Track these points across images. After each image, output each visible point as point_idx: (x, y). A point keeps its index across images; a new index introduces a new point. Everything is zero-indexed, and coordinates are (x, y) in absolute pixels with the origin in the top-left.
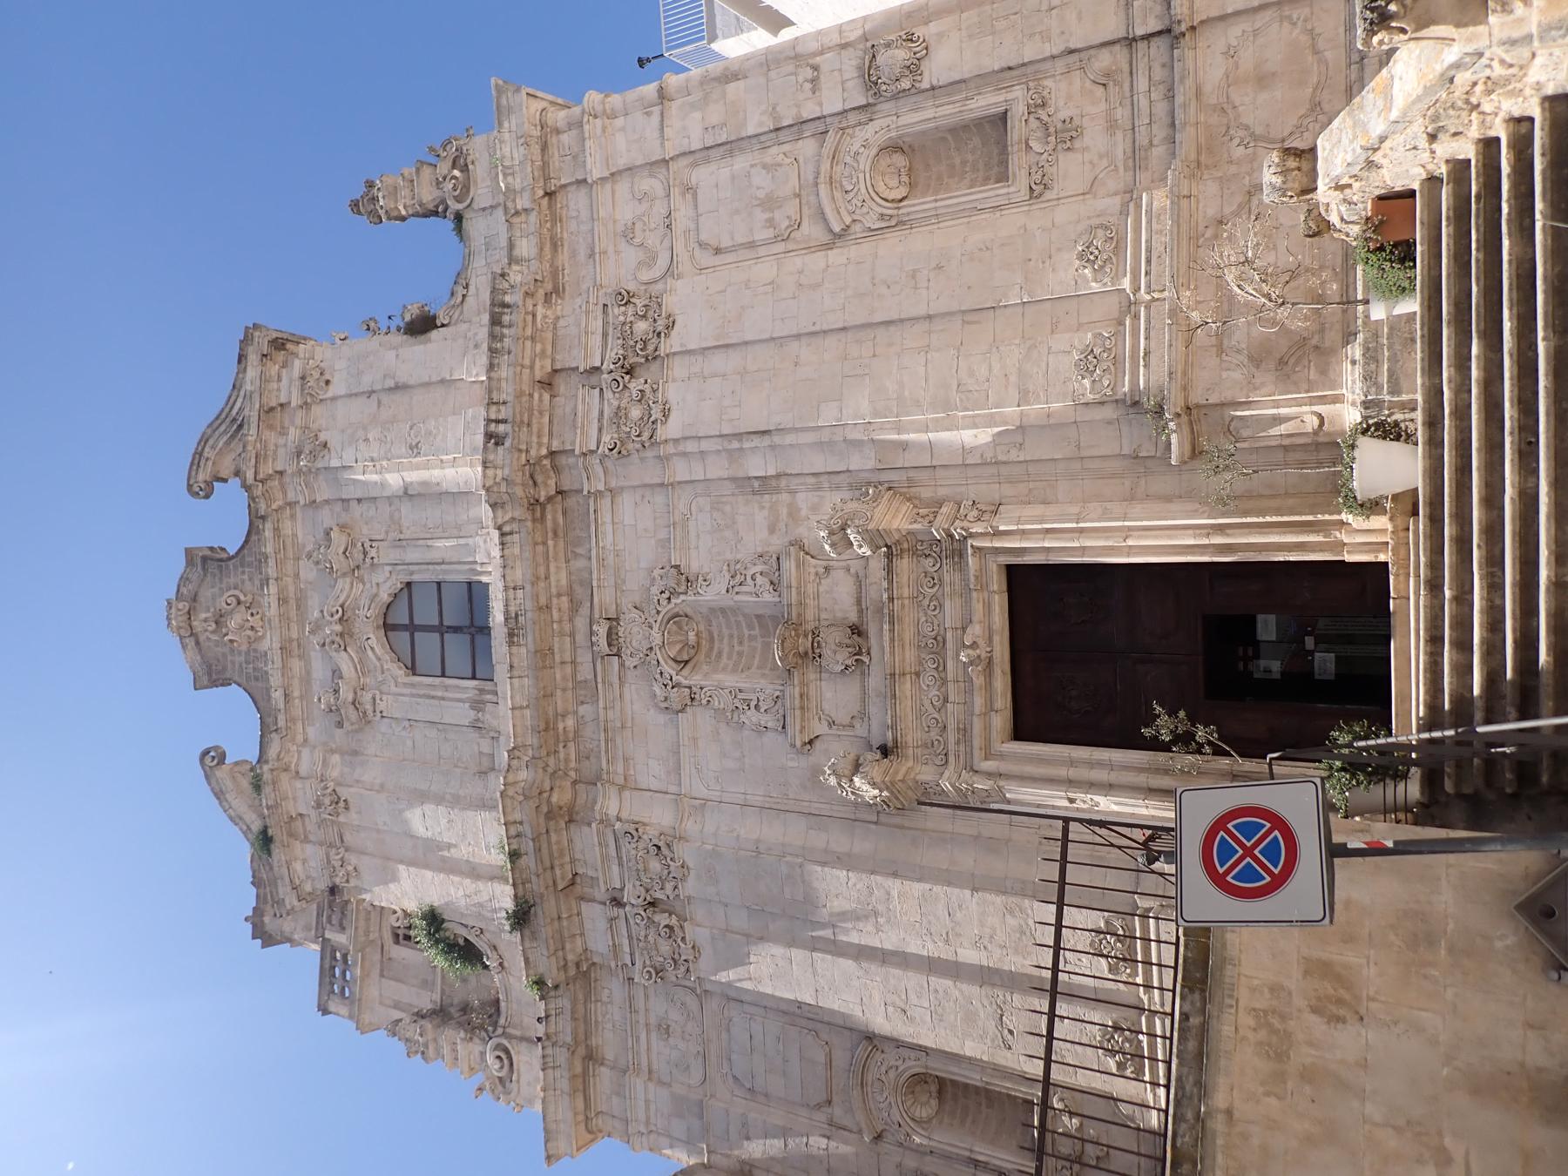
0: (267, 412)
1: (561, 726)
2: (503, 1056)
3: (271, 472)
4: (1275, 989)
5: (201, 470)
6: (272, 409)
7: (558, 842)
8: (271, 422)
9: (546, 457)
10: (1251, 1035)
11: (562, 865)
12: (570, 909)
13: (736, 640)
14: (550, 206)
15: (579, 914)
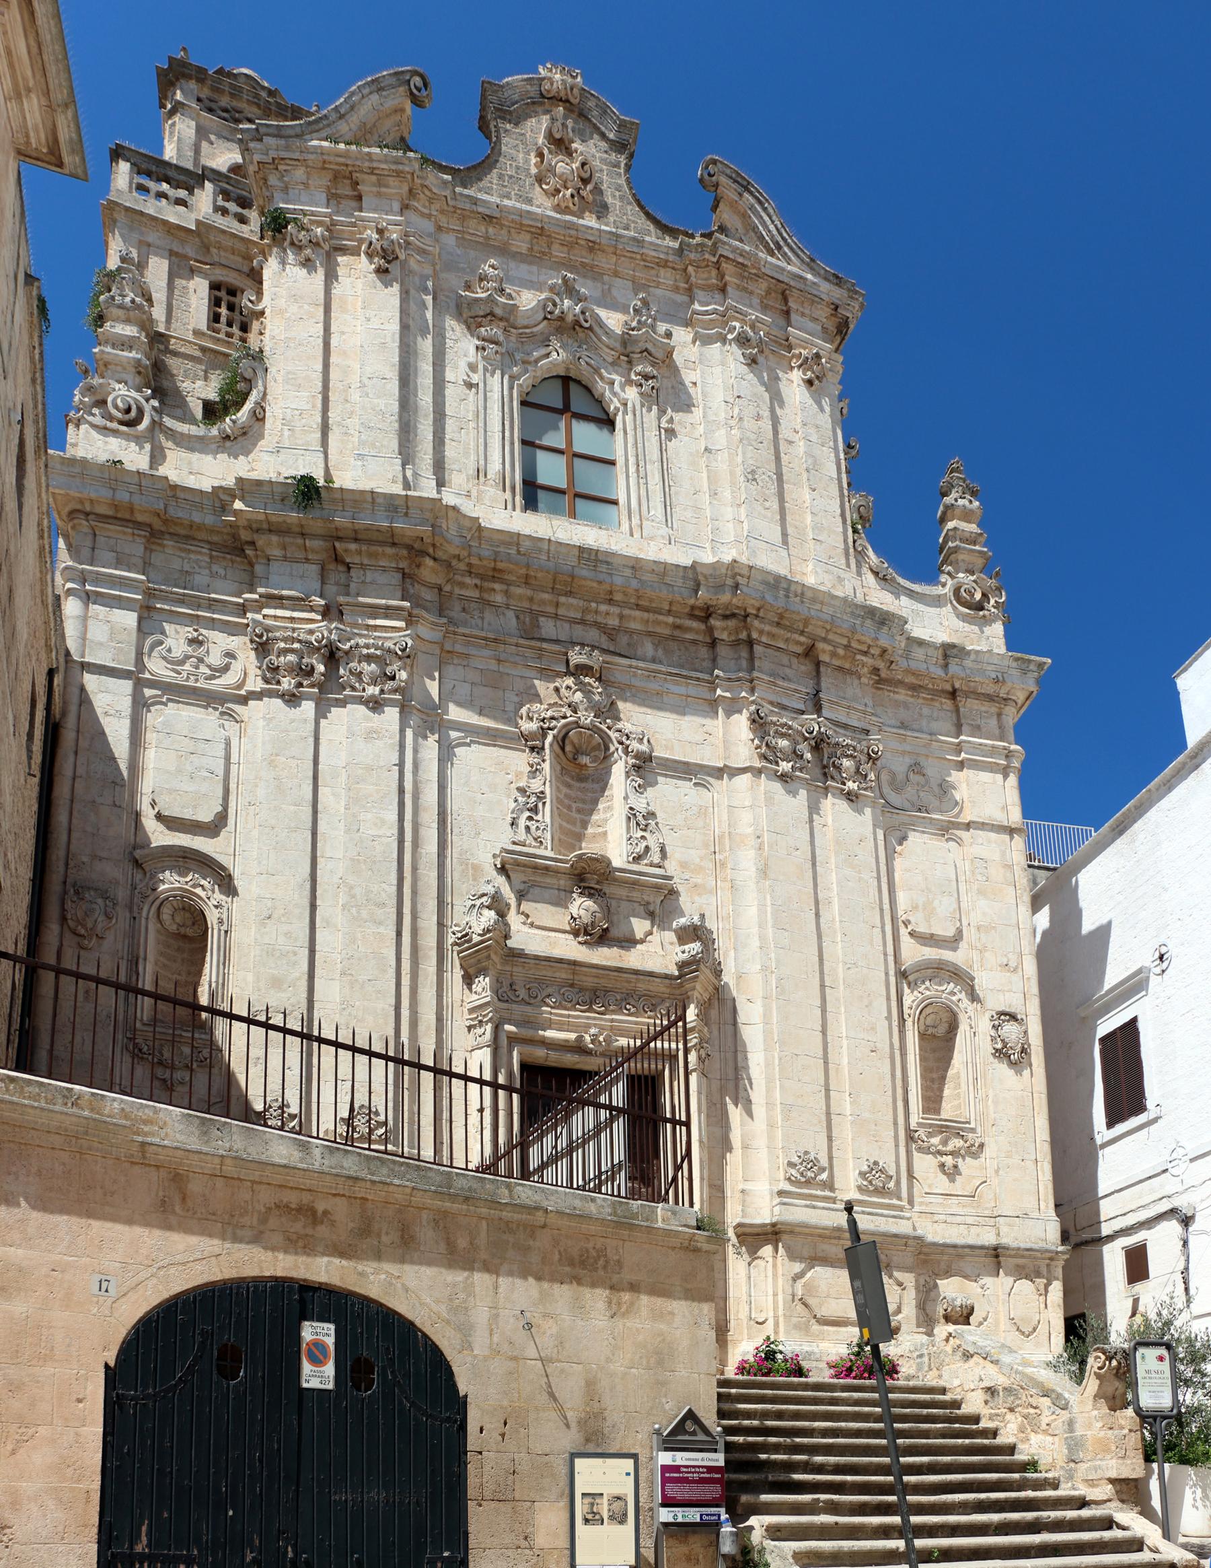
0: (783, 293)
1: (497, 586)
2: (127, 417)
3: (727, 278)
4: (619, 1263)
5: (730, 182)
6: (785, 300)
7: (384, 554)
8: (773, 295)
9: (749, 636)
10: (590, 1245)
11: (359, 552)
12: (313, 551)
13: (581, 805)
14: (943, 691)
15: (307, 560)
